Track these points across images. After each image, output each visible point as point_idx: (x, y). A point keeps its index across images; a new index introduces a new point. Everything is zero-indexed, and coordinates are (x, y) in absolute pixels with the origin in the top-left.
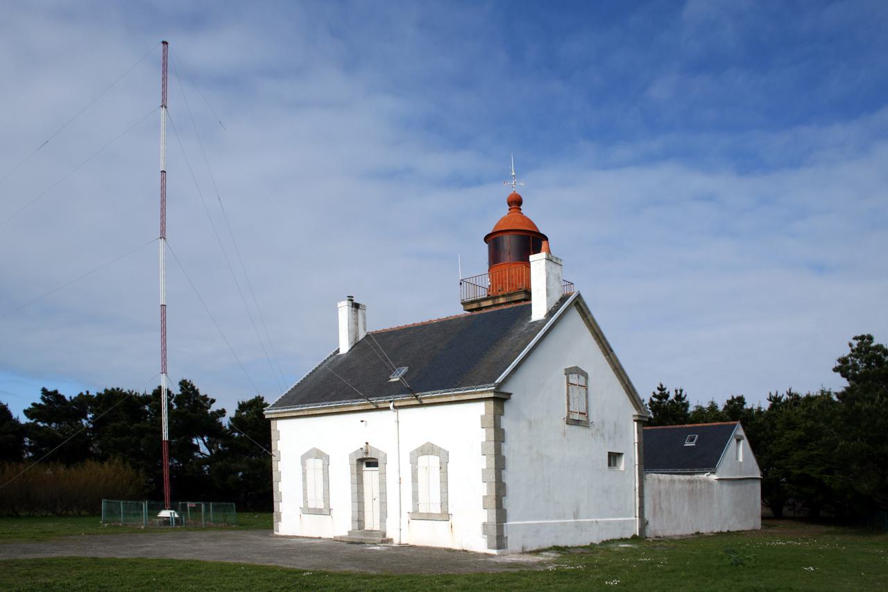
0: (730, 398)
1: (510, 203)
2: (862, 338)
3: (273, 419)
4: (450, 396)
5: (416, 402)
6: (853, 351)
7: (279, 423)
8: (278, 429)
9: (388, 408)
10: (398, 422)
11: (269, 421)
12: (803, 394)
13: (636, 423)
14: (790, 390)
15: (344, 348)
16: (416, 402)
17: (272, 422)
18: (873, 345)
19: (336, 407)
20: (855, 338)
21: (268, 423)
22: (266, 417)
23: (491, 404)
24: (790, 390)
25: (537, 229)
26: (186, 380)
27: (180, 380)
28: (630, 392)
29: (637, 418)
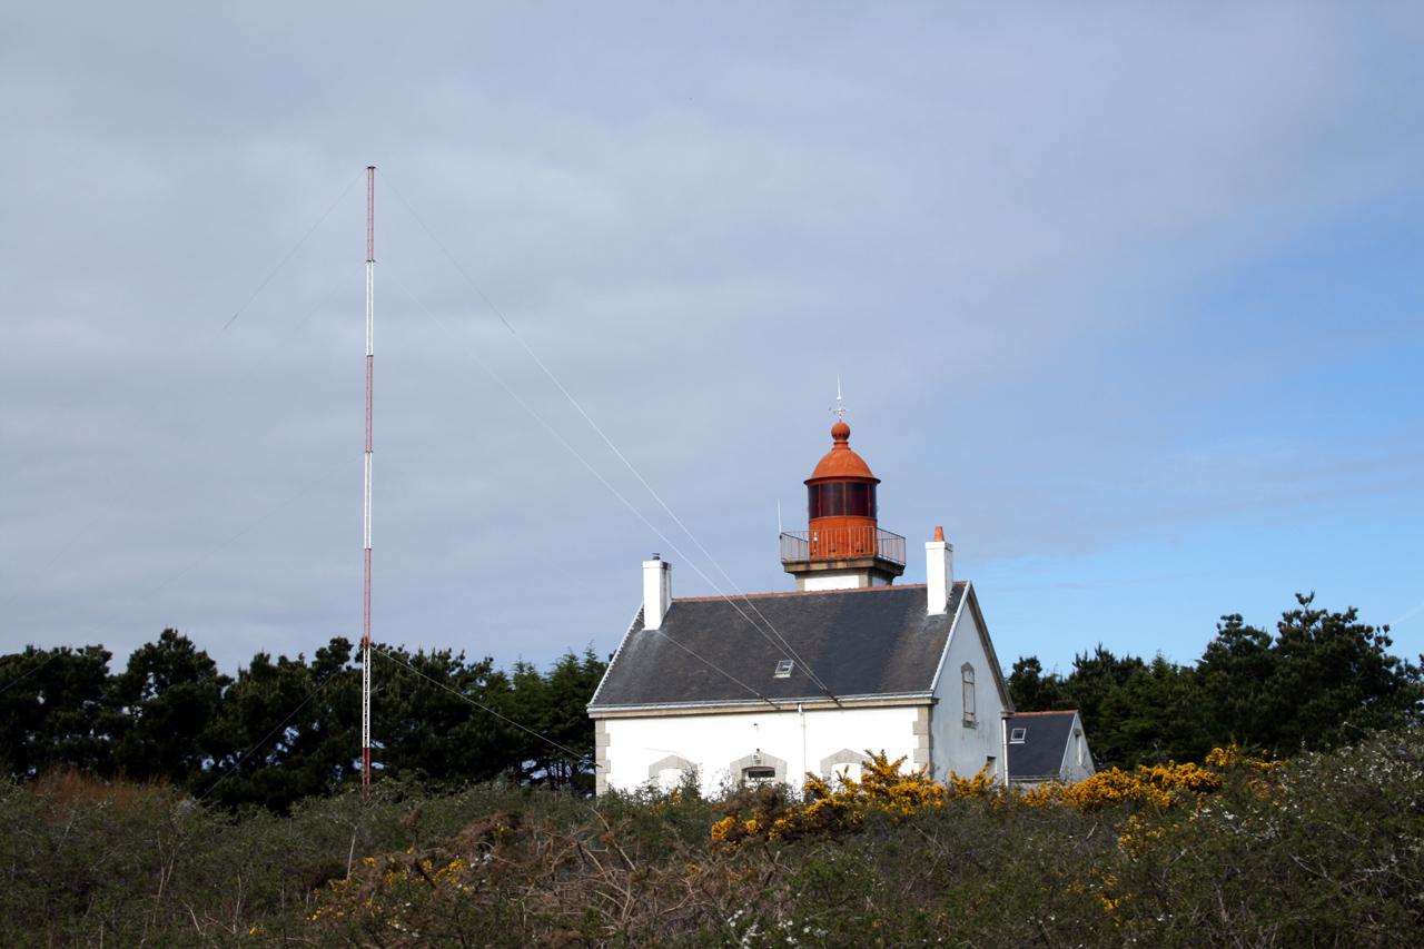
0: (1018, 662)
1: (835, 435)
2: (1231, 618)
3: (601, 719)
4: (878, 700)
5: (835, 705)
6: (1221, 633)
7: (608, 723)
8: (607, 732)
9: (796, 711)
10: (805, 726)
11: (593, 721)
12: (1119, 656)
13: (1004, 721)
14: (1100, 647)
15: (653, 621)
16: (835, 705)
17: (597, 723)
18: (1243, 627)
19: (715, 707)
20: (1223, 618)
21: (590, 725)
22: (591, 716)
23: (926, 711)
24: (1100, 647)
25: (868, 471)
26: (171, 630)
27: (282, 654)
28: (665, 589)
29: (1005, 715)
